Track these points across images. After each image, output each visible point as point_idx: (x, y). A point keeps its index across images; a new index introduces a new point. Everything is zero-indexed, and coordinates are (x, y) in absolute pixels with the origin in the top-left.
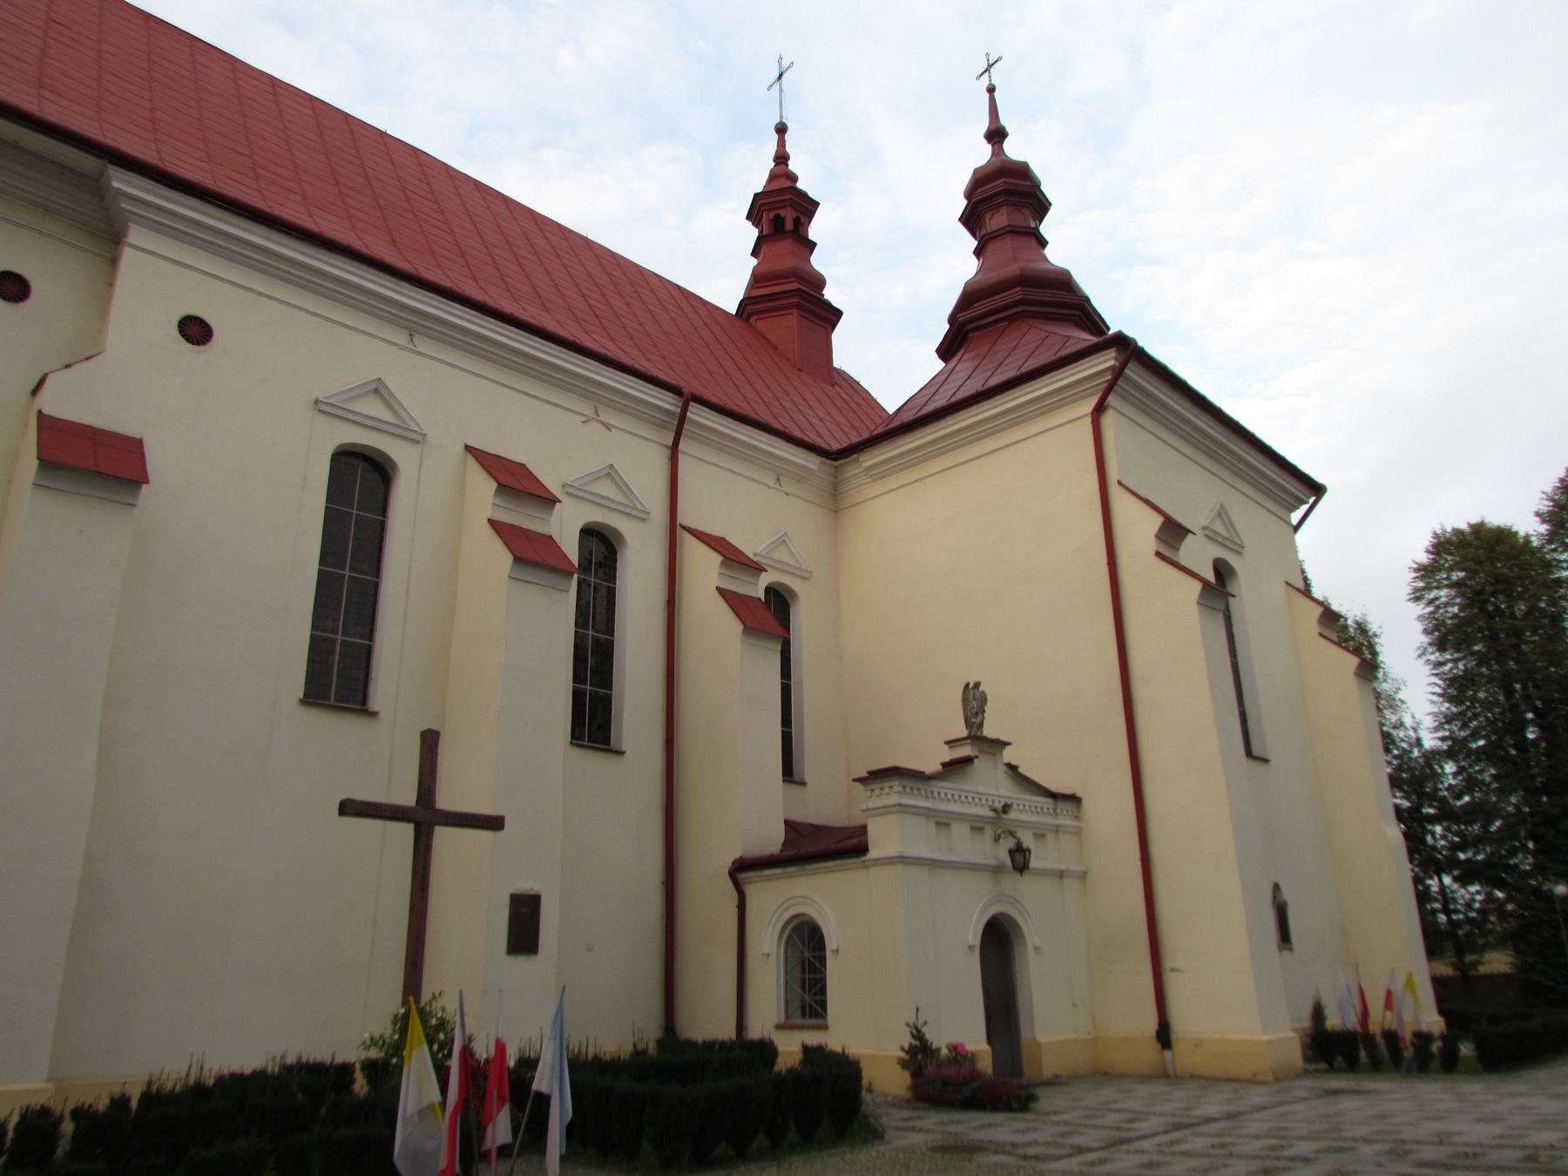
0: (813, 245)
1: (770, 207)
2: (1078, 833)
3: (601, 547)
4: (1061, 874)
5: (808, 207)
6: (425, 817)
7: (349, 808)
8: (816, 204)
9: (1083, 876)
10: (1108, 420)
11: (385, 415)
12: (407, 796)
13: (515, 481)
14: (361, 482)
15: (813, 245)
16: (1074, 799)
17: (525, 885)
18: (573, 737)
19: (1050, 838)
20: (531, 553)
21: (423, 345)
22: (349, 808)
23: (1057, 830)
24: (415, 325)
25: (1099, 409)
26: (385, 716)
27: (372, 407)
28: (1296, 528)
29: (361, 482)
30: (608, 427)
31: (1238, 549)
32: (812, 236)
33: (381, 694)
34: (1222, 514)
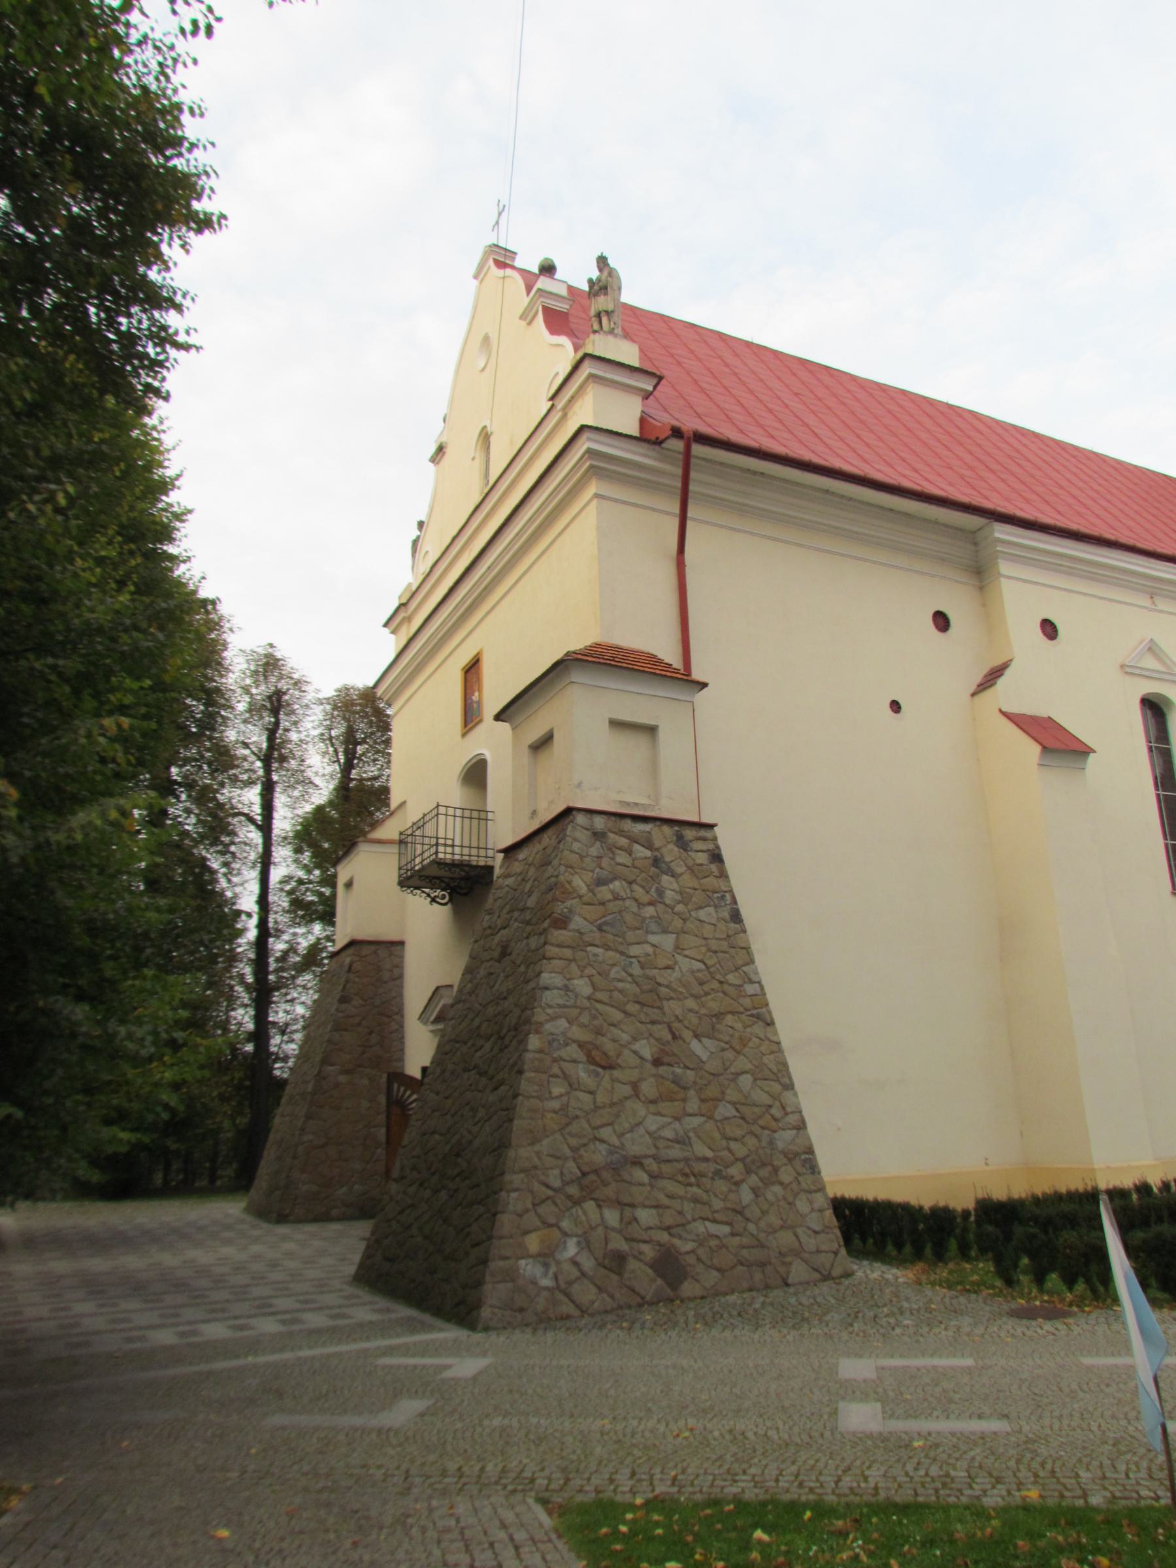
11: (1157, 666)
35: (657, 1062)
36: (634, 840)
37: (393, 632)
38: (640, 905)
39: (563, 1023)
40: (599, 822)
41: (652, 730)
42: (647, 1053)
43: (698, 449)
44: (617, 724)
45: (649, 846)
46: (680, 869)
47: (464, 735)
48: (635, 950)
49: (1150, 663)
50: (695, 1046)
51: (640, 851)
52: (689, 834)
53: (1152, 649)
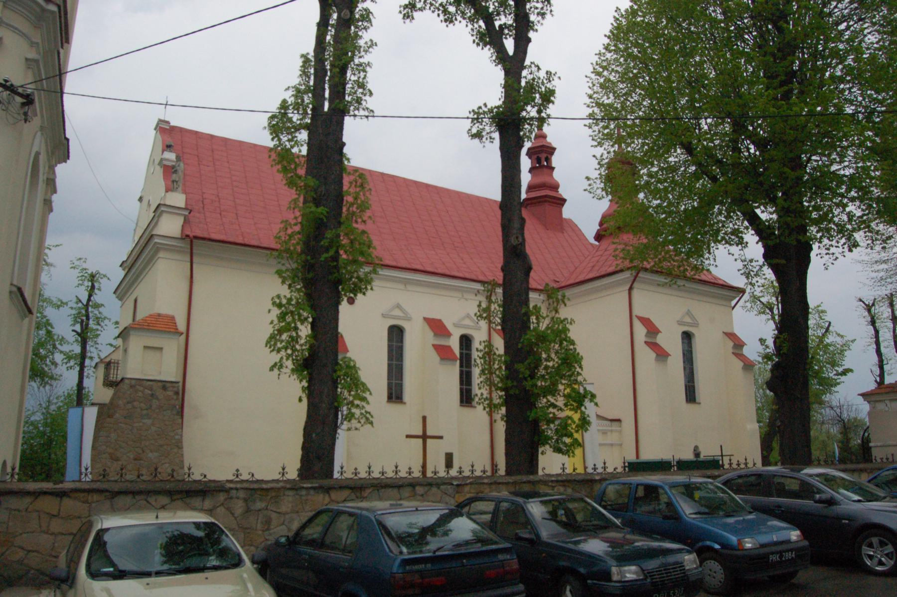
0: (553, 168)
1: (535, 153)
2: (621, 431)
3: (466, 341)
4: (612, 445)
5: (551, 150)
6: (424, 437)
7: (408, 436)
8: (554, 149)
9: (621, 445)
10: (635, 293)
11: (401, 314)
12: (429, 441)
13: (437, 327)
14: (396, 334)
15: (553, 168)
16: (619, 420)
17: (449, 451)
18: (462, 401)
19: (609, 434)
20: (443, 352)
21: (409, 287)
22: (408, 436)
23: (612, 431)
24: (406, 282)
25: (631, 289)
26: (408, 403)
27: (397, 312)
28: (733, 308)
29: (396, 334)
30: (466, 299)
31: (696, 325)
32: (553, 165)
33: (406, 397)
34: (688, 313)
35: (135, 459)
36: (146, 388)
37: (121, 299)
38: (142, 410)
39: (104, 447)
40: (133, 382)
41: (161, 349)
42: (132, 457)
43: (194, 241)
44: (145, 347)
45: (151, 390)
46: (161, 397)
47: (425, 319)
48: (137, 425)
49: (397, 312)
50: (150, 455)
51: (148, 392)
52: (168, 385)
53: (398, 306)
